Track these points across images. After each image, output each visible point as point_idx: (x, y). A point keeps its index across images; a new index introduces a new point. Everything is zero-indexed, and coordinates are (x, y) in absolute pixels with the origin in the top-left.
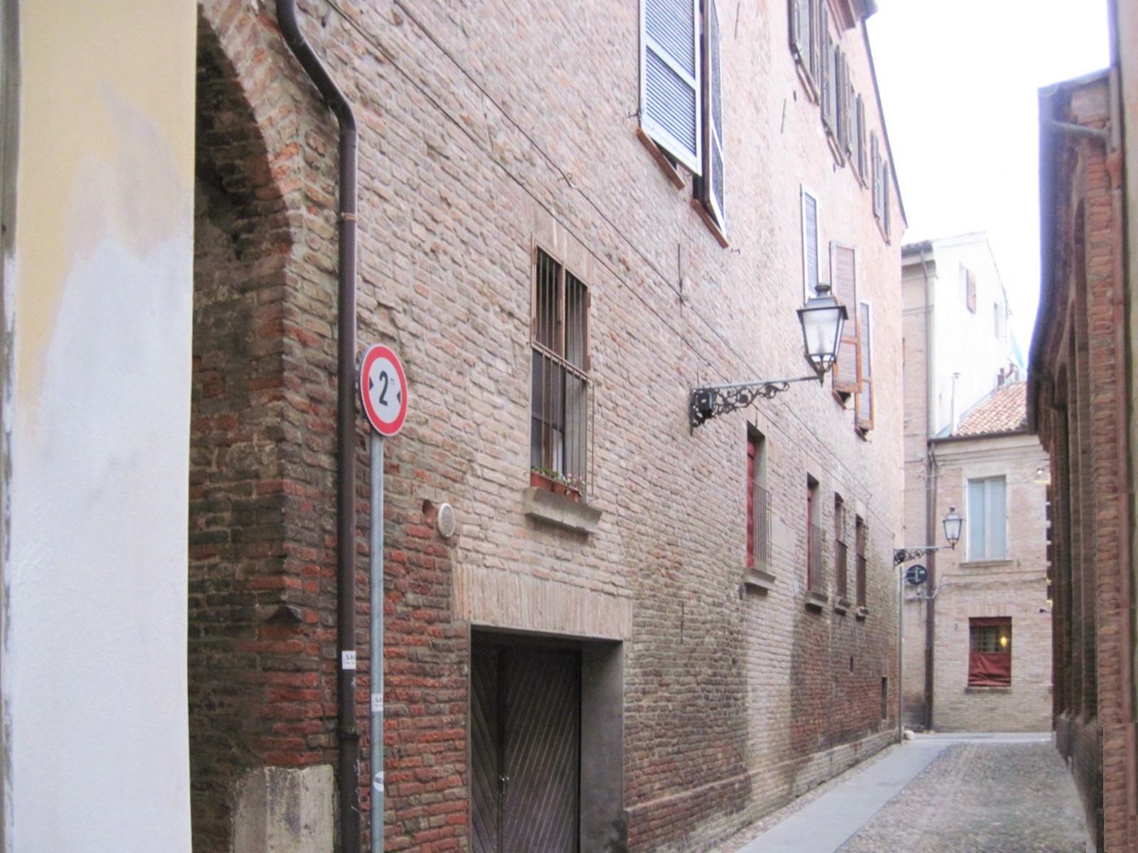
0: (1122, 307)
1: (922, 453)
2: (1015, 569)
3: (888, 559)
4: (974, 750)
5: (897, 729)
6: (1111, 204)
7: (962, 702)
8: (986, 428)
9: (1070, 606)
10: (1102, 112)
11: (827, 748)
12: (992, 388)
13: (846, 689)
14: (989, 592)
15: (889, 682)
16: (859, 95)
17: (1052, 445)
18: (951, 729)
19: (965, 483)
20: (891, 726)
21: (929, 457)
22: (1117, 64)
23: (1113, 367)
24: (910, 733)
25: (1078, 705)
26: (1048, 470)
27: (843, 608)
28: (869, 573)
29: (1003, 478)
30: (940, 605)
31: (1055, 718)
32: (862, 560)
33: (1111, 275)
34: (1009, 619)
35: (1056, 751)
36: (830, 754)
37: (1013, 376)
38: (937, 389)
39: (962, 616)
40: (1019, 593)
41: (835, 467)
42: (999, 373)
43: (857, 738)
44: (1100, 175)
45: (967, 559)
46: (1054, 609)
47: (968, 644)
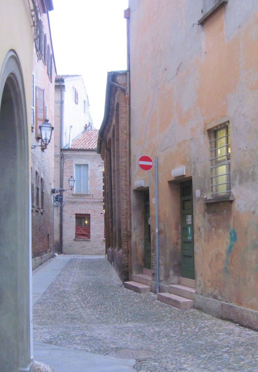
0: (128, 137)
1: (58, 153)
2: (91, 198)
3: (49, 192)
4: (80, 260)
5: (52, 253)
6: (126, 108)
7: (73, 244)
8: (81, 147)
9: (112, 215)
10: (125, 82)
11: (34, 258)
12: (83, 131)
13: (38, 238)
14: (82, 205)
15: (49, 236)
16: (45, 34)
17: (105, 159)
18: (69, 254)
19: (74, 165)
20: (50, 251)
21: (61, 155)
22: (129, 71)
23: (126, 152)
24: (56, 254)
25: (115, 245)
26: (103, 166)
27: (38, 210)
28: (45, 197)
29: (87, 165)
30: (65, 208)
31: (106, 250)
32: (42, 193)
33: (126, 127)
34: (89, 215)
35: (107, 261)
36: (35, 260)
37: (90, 127)
38: (64, 131)
39: (73, 213)
40: (93, 206)
41: (36, 162)
42: (85, 126)
43: (42, 255)
44: (124, 99)
45: (74, 193)
46: (105, 213)
47: (75, 223)
